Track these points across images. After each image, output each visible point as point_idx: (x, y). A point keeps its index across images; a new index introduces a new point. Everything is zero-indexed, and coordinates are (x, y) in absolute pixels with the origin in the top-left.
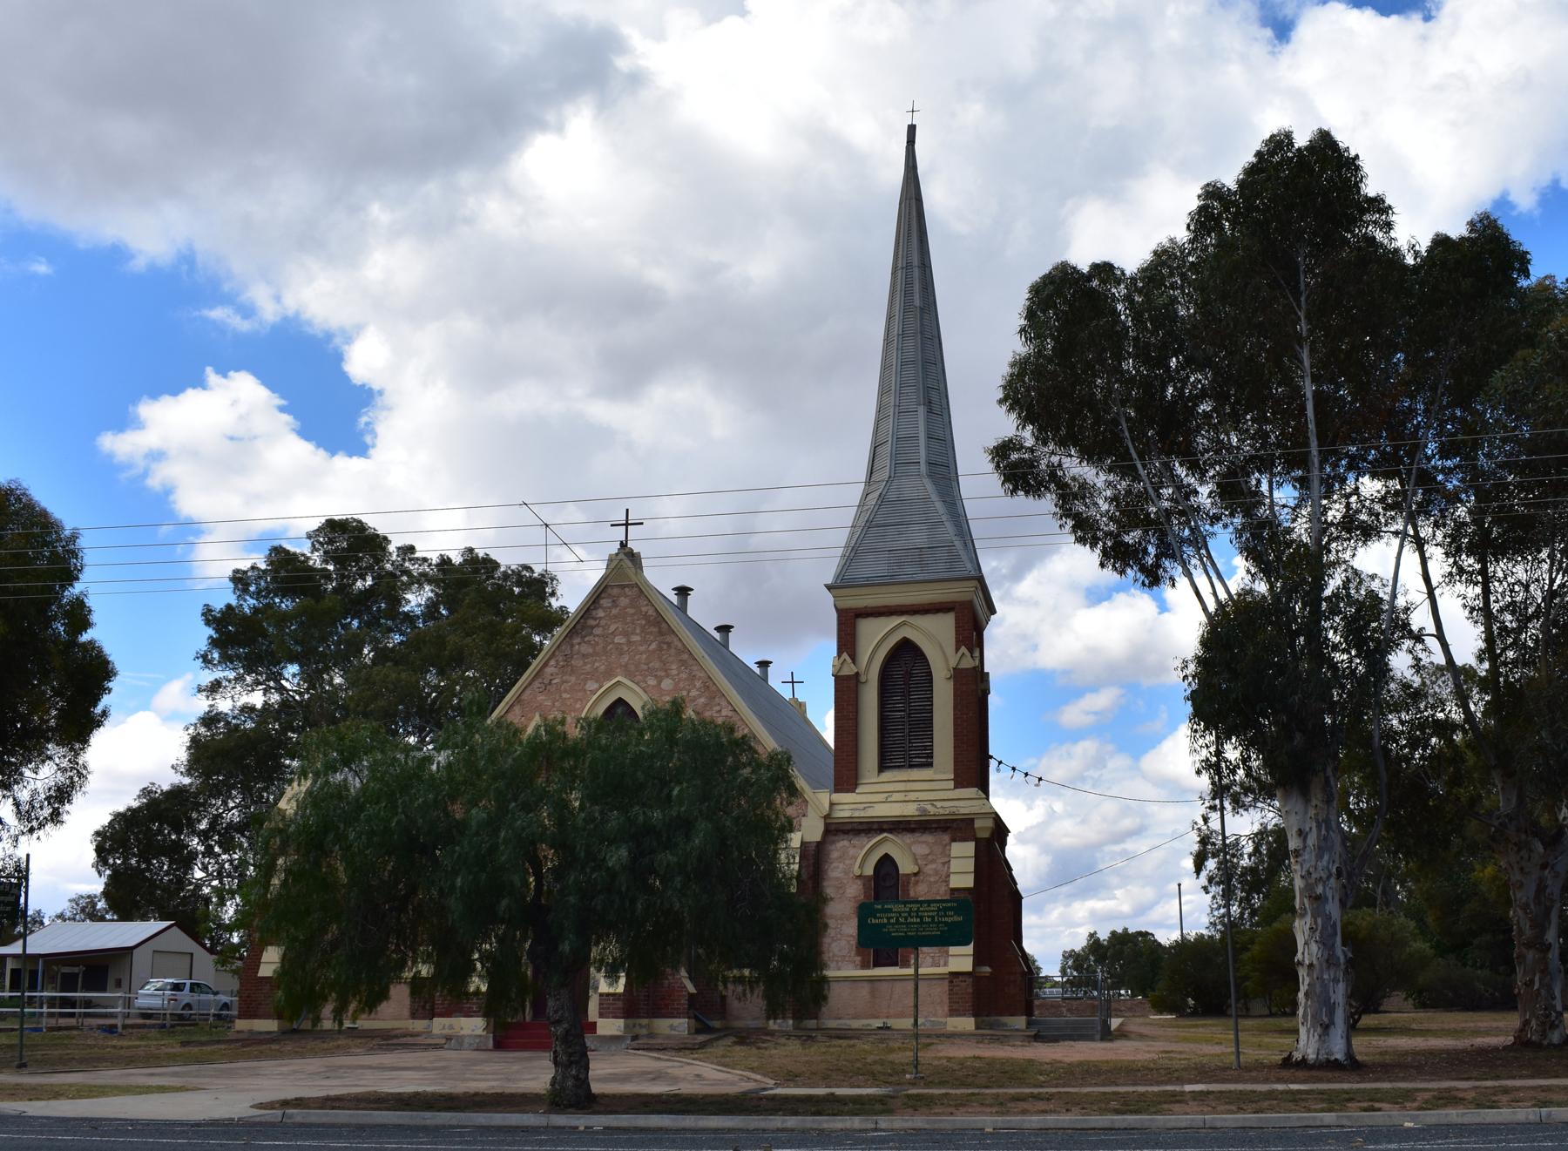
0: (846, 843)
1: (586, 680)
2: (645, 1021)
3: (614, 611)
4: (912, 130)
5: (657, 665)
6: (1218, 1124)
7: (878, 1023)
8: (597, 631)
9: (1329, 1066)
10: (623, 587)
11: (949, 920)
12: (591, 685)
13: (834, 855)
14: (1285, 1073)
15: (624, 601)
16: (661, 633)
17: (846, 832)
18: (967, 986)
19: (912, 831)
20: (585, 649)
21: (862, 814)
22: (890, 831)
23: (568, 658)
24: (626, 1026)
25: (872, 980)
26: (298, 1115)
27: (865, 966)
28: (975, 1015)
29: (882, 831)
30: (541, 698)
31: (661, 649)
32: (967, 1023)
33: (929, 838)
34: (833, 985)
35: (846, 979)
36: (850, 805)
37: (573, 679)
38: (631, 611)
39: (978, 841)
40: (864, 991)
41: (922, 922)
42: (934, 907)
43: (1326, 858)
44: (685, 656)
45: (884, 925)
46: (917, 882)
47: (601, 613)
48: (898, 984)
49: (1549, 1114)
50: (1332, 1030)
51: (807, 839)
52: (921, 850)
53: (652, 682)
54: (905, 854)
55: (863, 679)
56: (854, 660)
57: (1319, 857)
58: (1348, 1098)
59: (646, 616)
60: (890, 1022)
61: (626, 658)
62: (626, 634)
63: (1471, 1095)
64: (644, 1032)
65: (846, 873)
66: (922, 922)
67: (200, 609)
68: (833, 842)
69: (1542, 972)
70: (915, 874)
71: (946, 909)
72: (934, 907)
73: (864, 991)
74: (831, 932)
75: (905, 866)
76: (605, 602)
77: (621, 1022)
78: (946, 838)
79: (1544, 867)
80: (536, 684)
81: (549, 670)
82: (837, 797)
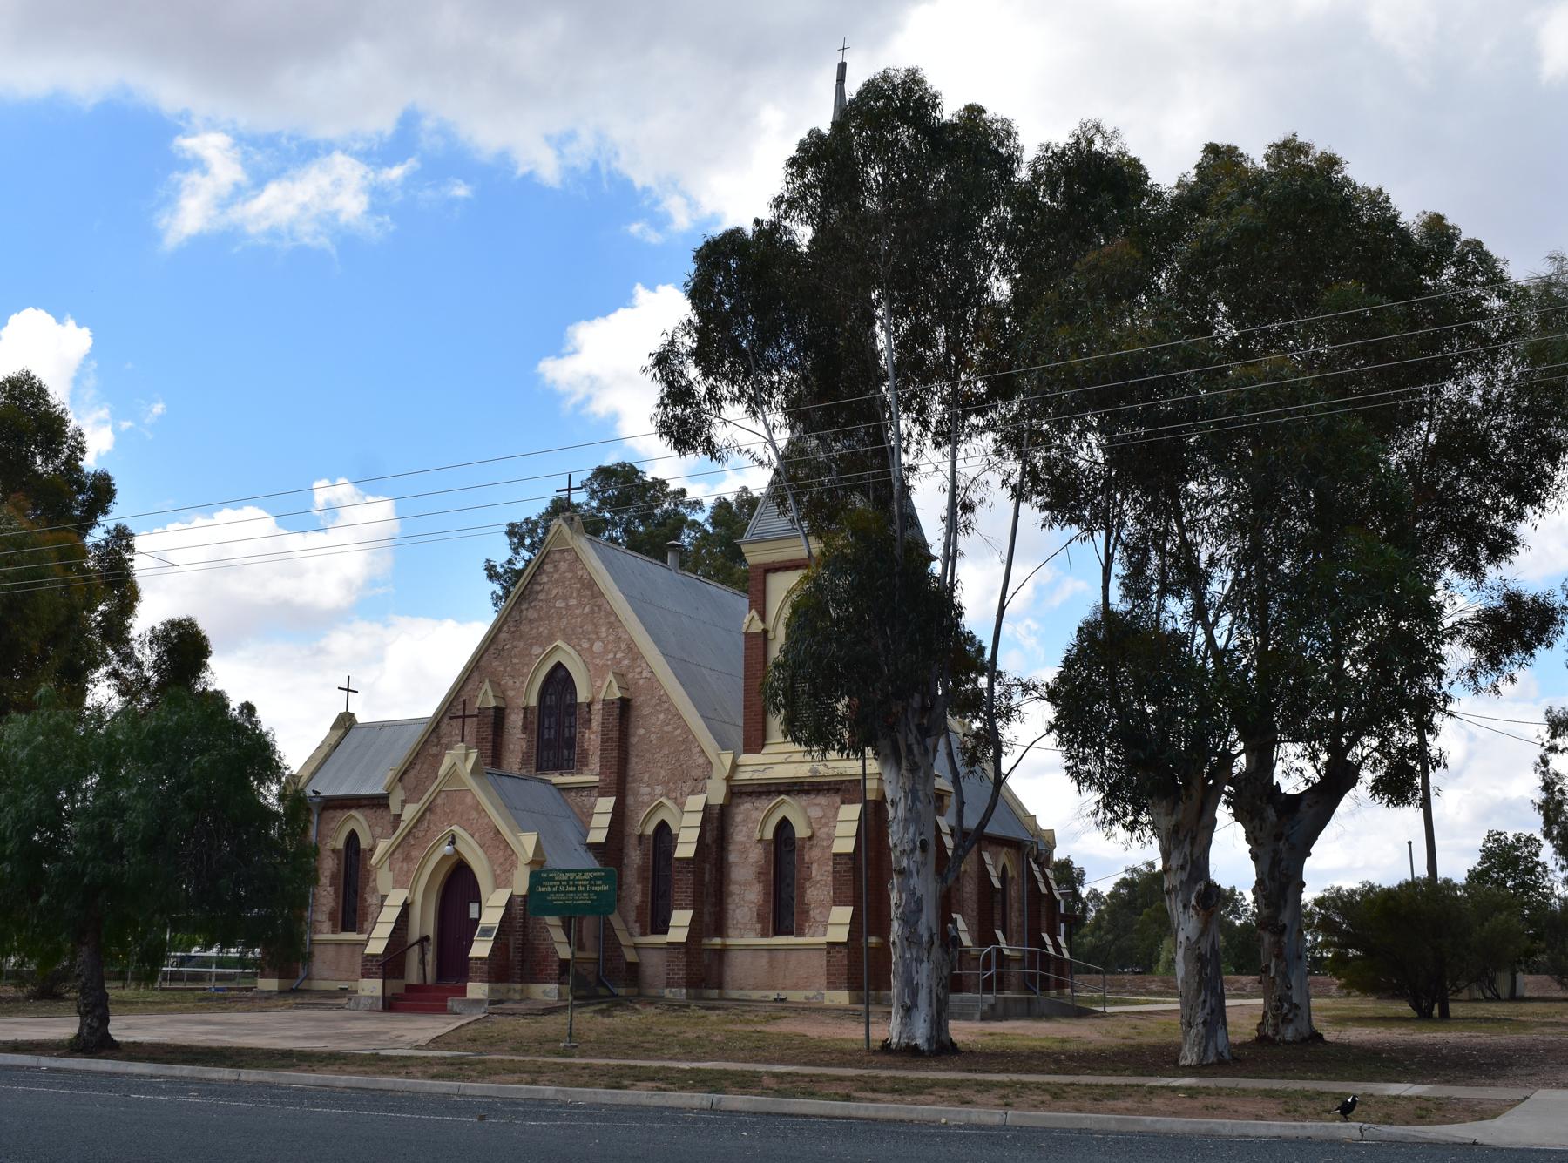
0: (748, 806)
1: (531, 645)
2: (518, 986)
3: (556, 576)
4: (842, 67)
5: (589, 627)
6: (468, 1092)
7: (773, 995)
8: (542, 596)
9: (910, 1053)
10: (563, 551)
11: (598, 889)
12: (536, 650)
13: (739, 818)
14: (887, 1059)
15: (563, 566)
16: (594, 596)
17: (750, 794)
18: (842, 956)
19: (807, 792)
20: (532, 614)
21: (761, 776)
22: (788, 793)
23: (518, 623)
24: (491, 990)
25: (771, 949)
26: (870, 1095)
27: (764, 934)
28: (849, 989)
29: (780, 793)
30: (495, 663)
31: (592, 612)
32: (842, 997)
33: (822, 800)
34: (732, 954)
35: (748, 948)
36: (755, 767)
37: (521, 644)
38: (569, 575)
39: (866, 803)
40: (763, 960)
41: (577, 891)
42: (587, 876)
43: (912, 829)
44: (612, 619)
45: (547, 893)
46: (811, 847)
47: (544, 579)
48: (794, 954)
49: (719, 1101)
50: (915, 1012)
51: (711, 802)
52: (815, 813)
53: (585, 645)
54: (798, 813)
55: (771, 636)
56: (763, 619)
57: (906, 829)
58: (1113, 1092)
59: (581, 579)
60: (784, 994)
61: (564, 623)
62: (565, 598)
63: (887, 1085)
64: (517, 997)
65: (749, 837)
66: (577, 891)
67: (483, 564)
68: (738, 805)
69: (1277, 957)
70: (810, 838)
71: (596, 878)
72: (587, 876)
73: (763, 960)
74: (736, 898)
75: (801, 831)
76: (548, 568)
77: (485, 986)
78: (838, 799)
79: (1278, 838)
80: (492, 650)
81: (503, 636)
82: (745, 758)
